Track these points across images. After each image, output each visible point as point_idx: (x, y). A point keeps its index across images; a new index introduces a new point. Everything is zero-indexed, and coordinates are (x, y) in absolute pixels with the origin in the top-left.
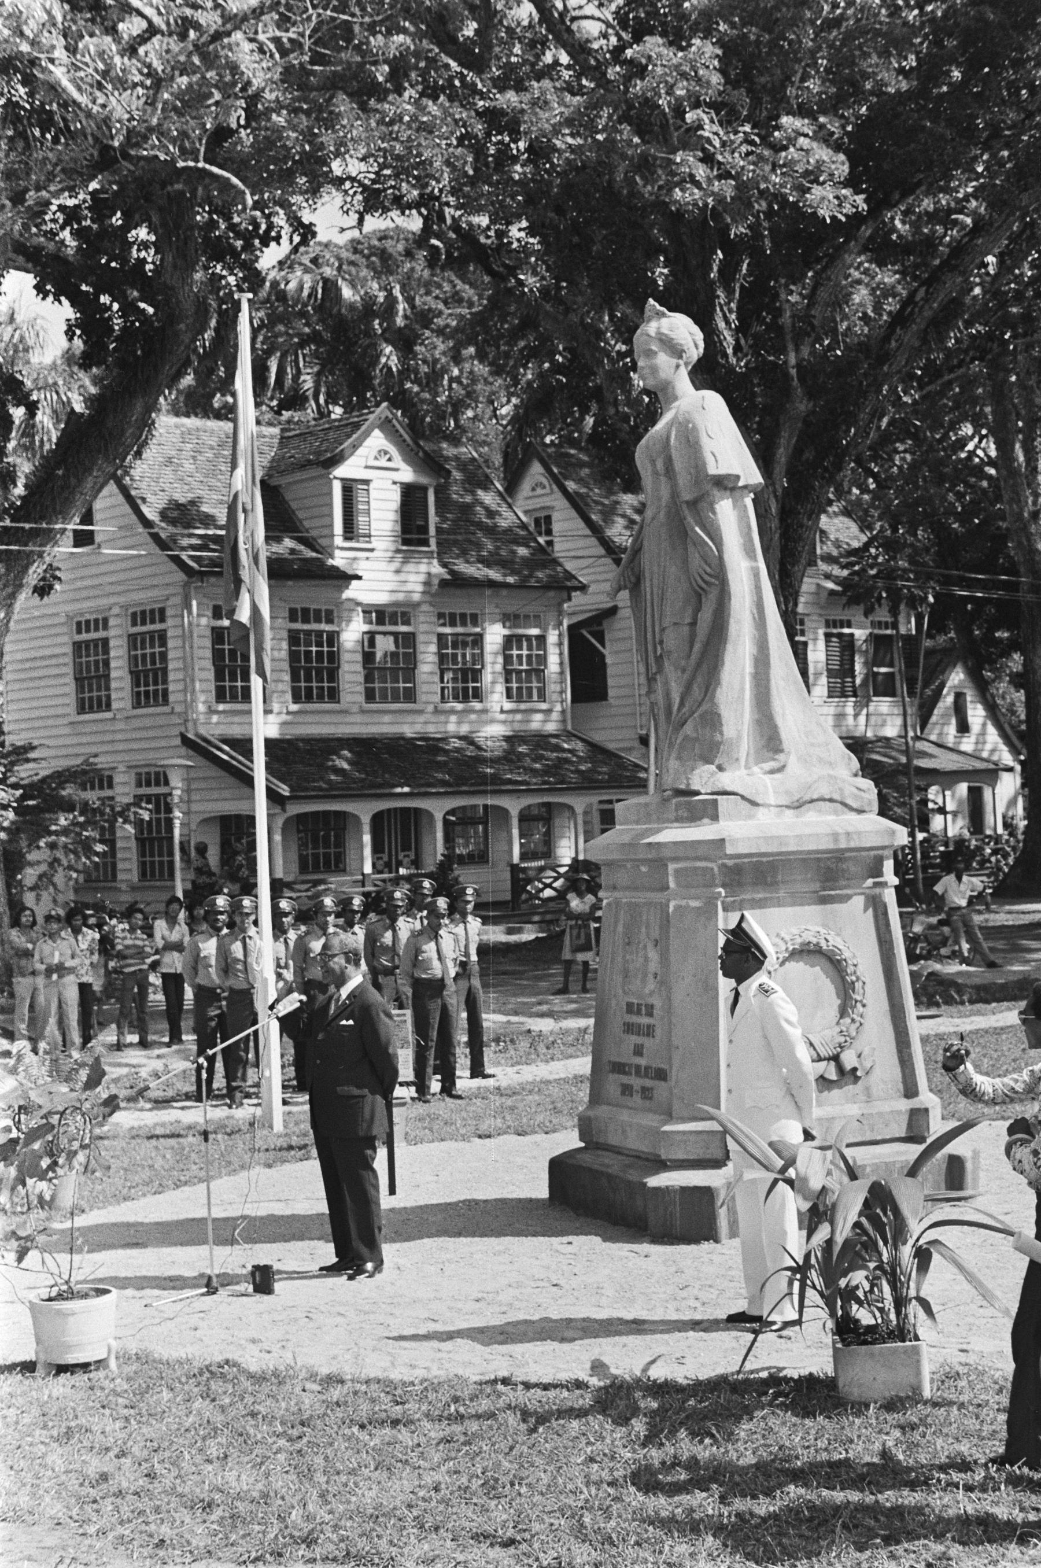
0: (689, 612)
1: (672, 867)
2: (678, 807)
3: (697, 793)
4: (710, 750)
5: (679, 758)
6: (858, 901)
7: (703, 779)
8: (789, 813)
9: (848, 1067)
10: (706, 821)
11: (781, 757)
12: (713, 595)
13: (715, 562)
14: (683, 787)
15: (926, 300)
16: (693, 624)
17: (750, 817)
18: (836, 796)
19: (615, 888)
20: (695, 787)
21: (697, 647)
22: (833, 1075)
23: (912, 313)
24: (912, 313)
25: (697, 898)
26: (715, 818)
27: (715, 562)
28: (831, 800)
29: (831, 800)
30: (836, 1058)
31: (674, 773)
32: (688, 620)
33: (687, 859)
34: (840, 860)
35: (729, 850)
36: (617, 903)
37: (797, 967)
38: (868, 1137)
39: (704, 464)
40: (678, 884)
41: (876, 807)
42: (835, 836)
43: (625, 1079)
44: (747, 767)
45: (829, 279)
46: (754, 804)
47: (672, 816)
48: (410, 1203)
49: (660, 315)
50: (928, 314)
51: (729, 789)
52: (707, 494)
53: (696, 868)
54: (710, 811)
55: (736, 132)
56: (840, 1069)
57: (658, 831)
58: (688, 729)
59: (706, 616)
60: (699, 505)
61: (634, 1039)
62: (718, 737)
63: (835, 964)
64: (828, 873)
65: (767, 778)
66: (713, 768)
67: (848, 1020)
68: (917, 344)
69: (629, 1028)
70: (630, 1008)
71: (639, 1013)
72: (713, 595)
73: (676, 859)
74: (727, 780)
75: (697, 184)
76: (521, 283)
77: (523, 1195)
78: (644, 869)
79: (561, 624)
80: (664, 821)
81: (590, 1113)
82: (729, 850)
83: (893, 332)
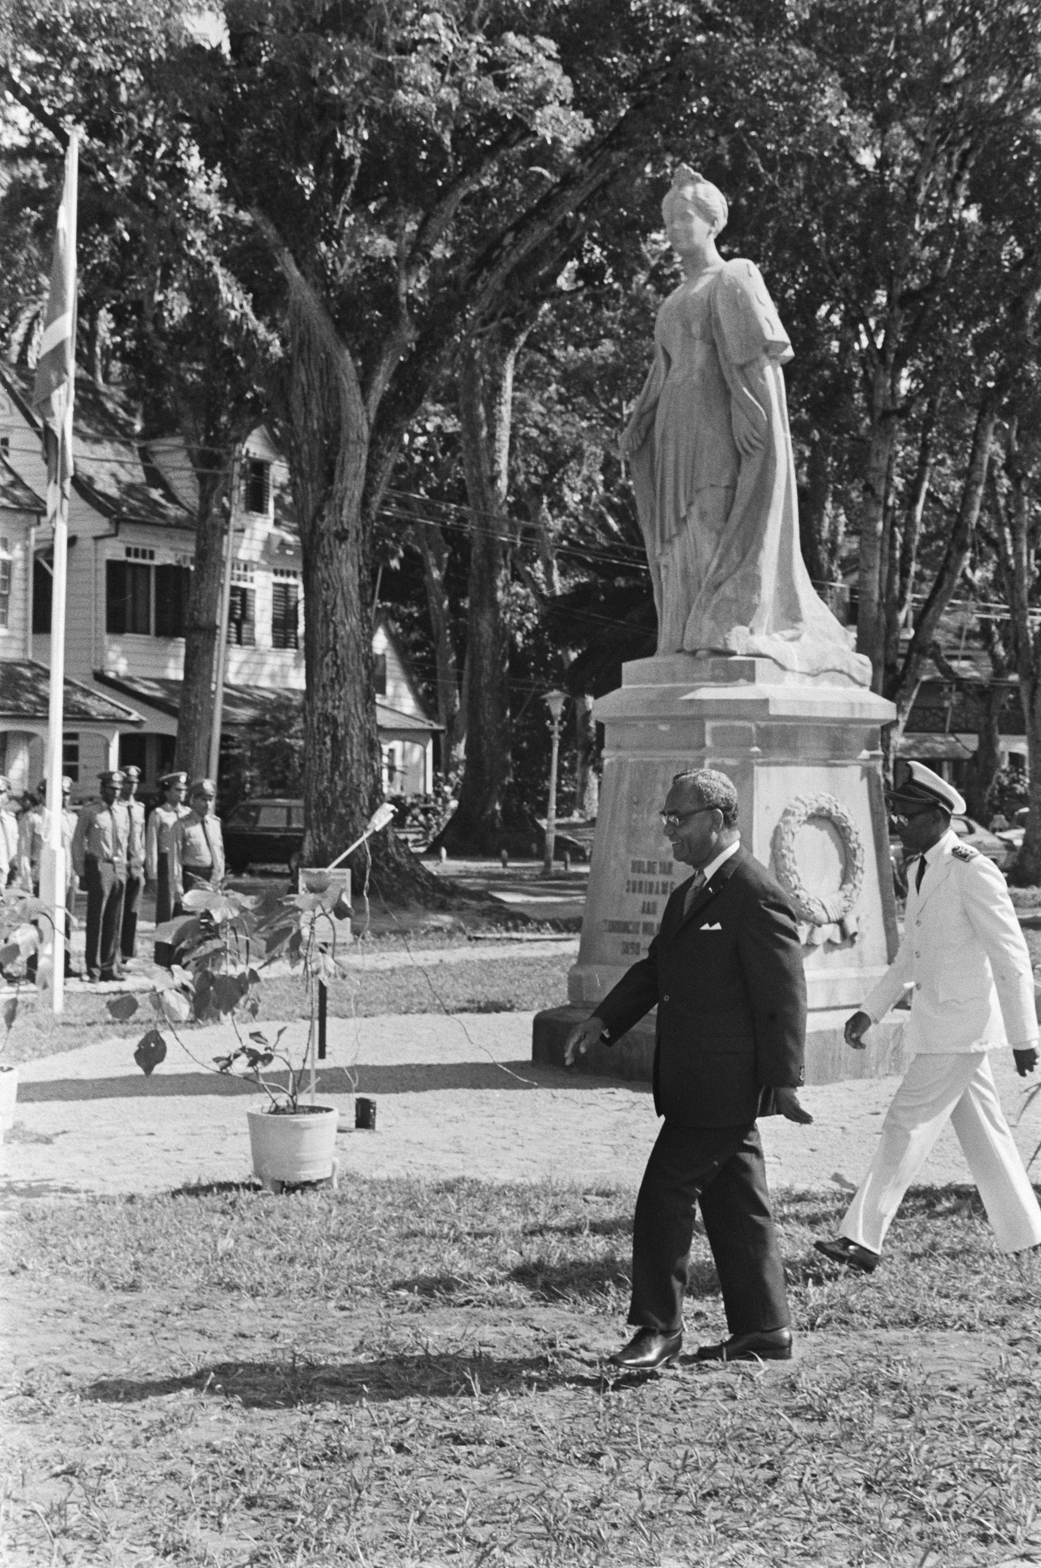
0: (727, 475)
1: (709, 725)
2: (714, 667)
3: (734, 654)
4: (745, 615)
5: (713, 618)
6: (857, 770)
7: (739, 640)
8: (808, 679)
9: (851, 931)
10: (742, 681)
11: (800, 625)
12: (758, 458)
13: (763, 427)
14: (720, 647)
15: (514, 245)
16: (732, 487)
17: (780, 681)
18: (845, 669)
19: (619, 747)
20: (733, 647)
21: (737, 510)
22: (837, 939)
23: (499, 257)
24: (499, 257)
25: (732, 757)
26: (751, 679)
27: (763, 427)
28: (841, 672)
29: (841, 672)
30: (840, 923)
31: (702, 631)
32: (725, 483)
33: (726, 717)
34: (845, 730)
35: (773, 711)
36: (621, 764)
37: (811, 830)
38: (834, 1004)
39: (760, 330)
40: (714, 740)
41: (869, 683)
42: (852, 705)
43: (627, 938)
44: (768, 634)
45: (442, 211)
46: (783, 668)
47: (707, 674)
48: (333, 1065)
49: (694, 180)
50: (514, 259)
51: (764, 651)
52: (757, 359)
53: (732, 728)
54: (746, 672)
55: (470, 41)
56: (844, 933)
57: (692, 689)
58: (727, 590)
59: (747, 481)
60: (748, 370)
61: (641, 898)
62: (756, 600)
63: (840, 831)
64: (833, 740)
65: (790, 644)
66: (746, 629)
67: (850, 886)
68: (500, 288)
69: (635, 887)
70: (637, 867)
71: (651, 870)
72: (758, 458)
73: (717, 717)
74: (761, 642)
75: (424, 90)
76: (110, 180)
77: (457, 1059)
78: (663, 728)
79: (27, 537)
80: (695, 680)
81: (580, 972)
82: (773, 711)
83: (480, 273)
